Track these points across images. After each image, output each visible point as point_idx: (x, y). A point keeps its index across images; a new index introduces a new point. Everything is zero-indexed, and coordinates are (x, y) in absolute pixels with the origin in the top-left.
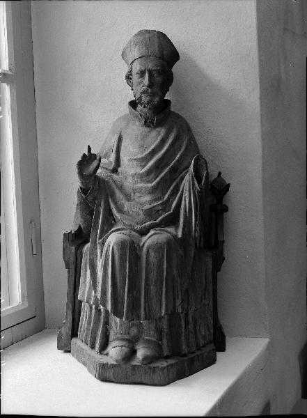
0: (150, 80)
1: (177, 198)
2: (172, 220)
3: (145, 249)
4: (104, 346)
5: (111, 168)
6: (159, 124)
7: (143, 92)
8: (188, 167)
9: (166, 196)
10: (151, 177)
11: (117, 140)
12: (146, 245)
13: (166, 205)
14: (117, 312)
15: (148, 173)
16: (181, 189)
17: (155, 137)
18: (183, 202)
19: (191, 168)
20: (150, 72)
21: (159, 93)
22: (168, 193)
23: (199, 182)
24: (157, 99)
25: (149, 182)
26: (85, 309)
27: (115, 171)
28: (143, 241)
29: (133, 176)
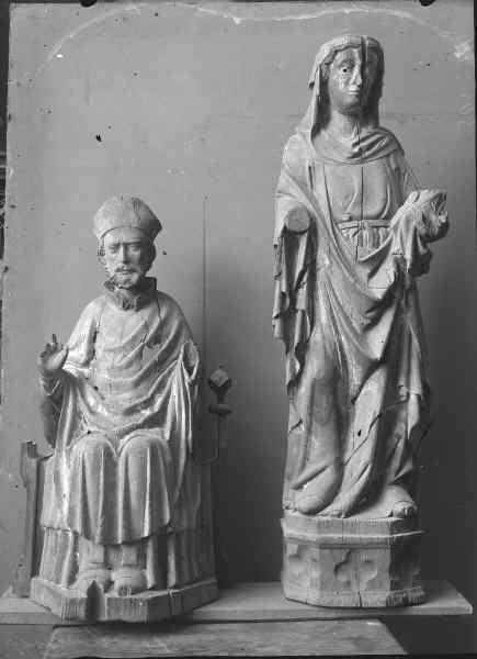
0: (126, 255)
1: (157, 382)
2: (156, 421)
3: (123, 454)
4: (72, 580)
5: (83, 360)
6: (140, 307)
7: (118, 270)
8: (177, 358)
9: (150, 393)
10: (141, 387)
11: (19, 464)
12: (125, 449)
13: (149, 403)
14: (87, 534)
15: (129, 364)
16: (168, 383)
17: (135, 321)
18: (170, 400)
19: (181, 356)
20: (126, 246)
21: (138, 269)
22: (154, 387)
23: (190, 373)
24: (135, 277)
25: (130, 376)
26: (49, 542)
27: (87, 364)
28: (121, 445)
29: (116, 247)
